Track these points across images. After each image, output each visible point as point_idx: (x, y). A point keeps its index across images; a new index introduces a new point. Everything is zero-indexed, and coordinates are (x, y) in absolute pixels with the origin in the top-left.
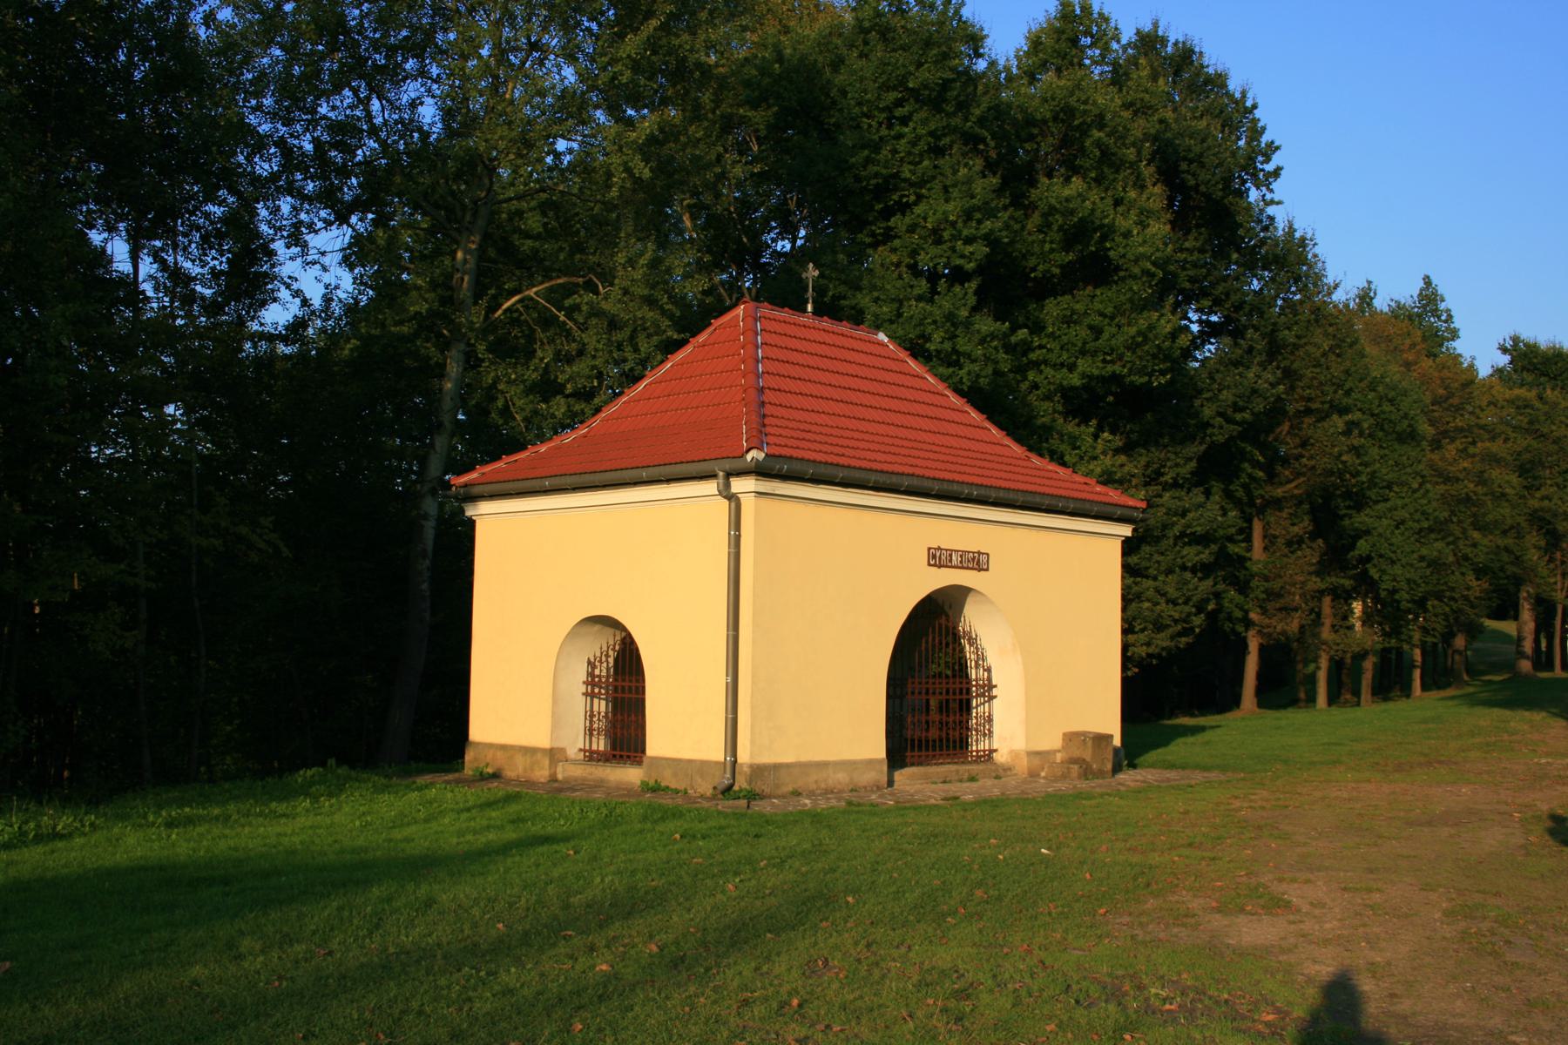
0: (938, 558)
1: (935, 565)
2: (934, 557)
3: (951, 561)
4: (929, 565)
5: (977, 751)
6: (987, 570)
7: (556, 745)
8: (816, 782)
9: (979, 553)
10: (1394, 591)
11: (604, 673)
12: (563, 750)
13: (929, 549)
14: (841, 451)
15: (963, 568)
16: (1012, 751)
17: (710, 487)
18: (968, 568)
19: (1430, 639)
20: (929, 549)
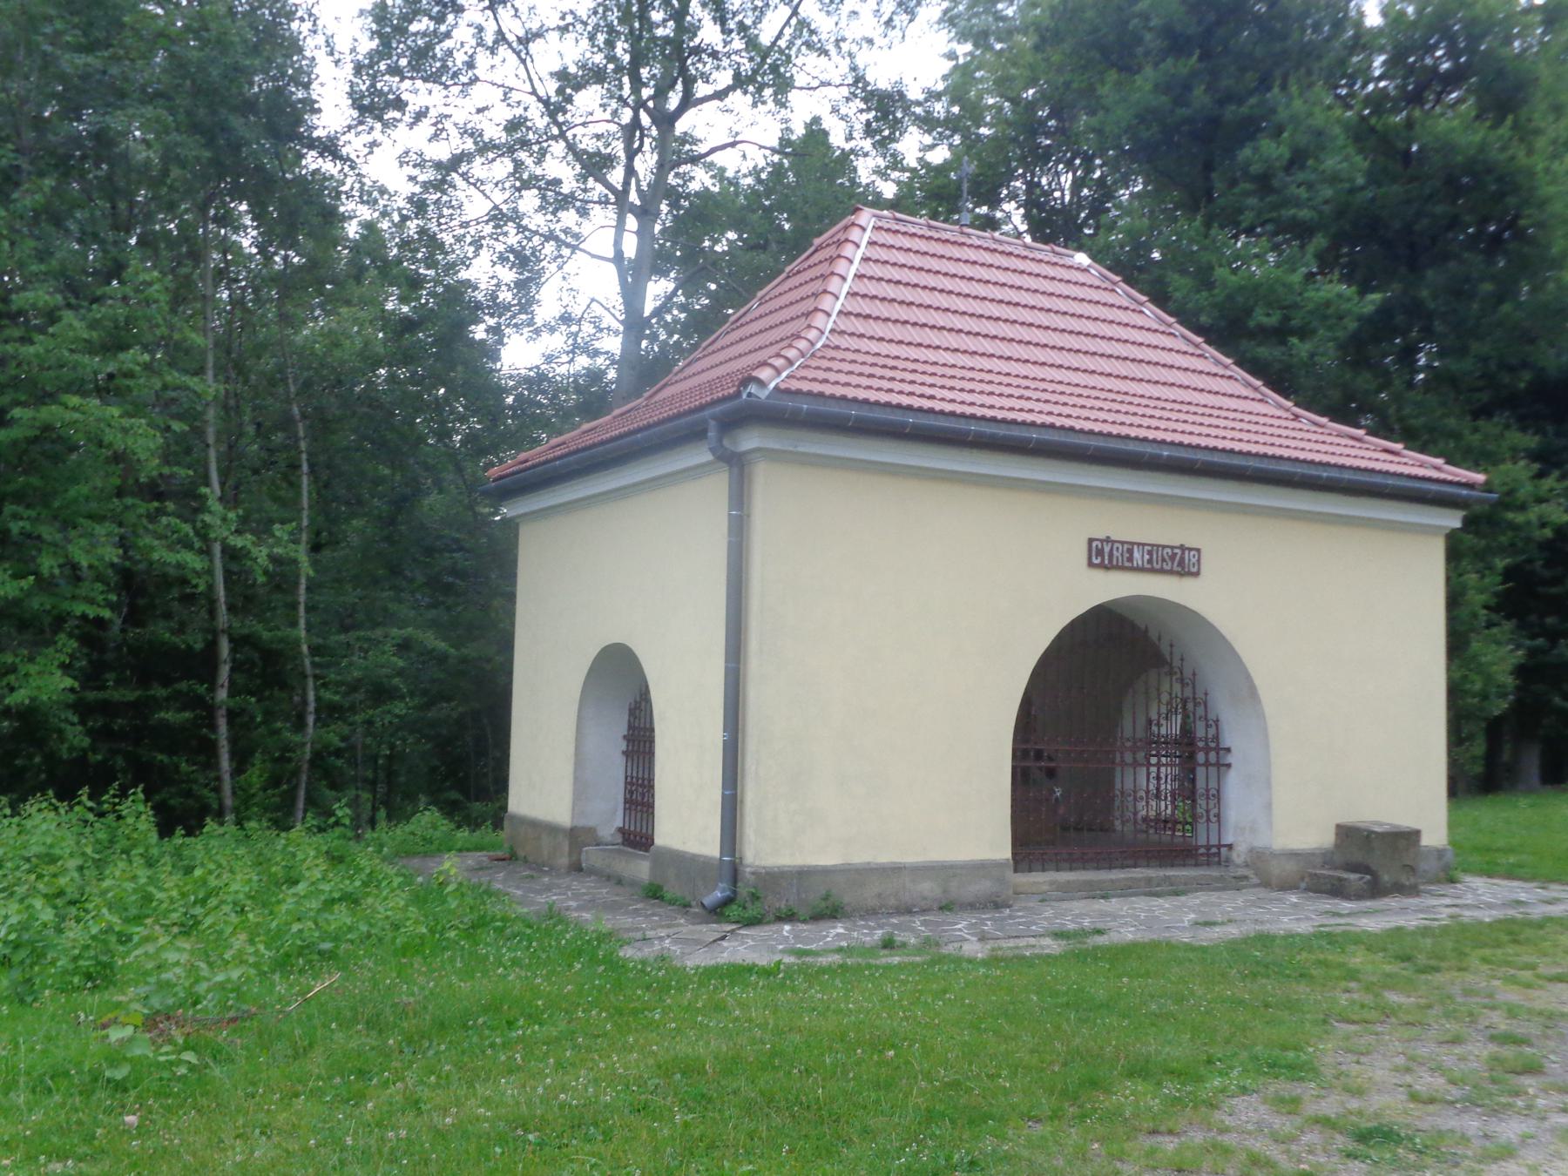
0: (1103, 555)
1: (1102, 566)
2: (1100, 553)
3: (1130, 559)
4: (1091, 564)
5: (1208, 847)
6: (1197, 574)
7: (582, 822)
8: (879, 895)
9: (1182, 547)
10: (22, 589)
11: (1166, 687)
12: (591, 831)
13: (1091, 541)
14: (1301, 444)
15: (1152, 571)
16: (1251, 850)
17: (700, 455)
18: (1162, 571)
19: (462, 1092)
20: (1091, 541)
